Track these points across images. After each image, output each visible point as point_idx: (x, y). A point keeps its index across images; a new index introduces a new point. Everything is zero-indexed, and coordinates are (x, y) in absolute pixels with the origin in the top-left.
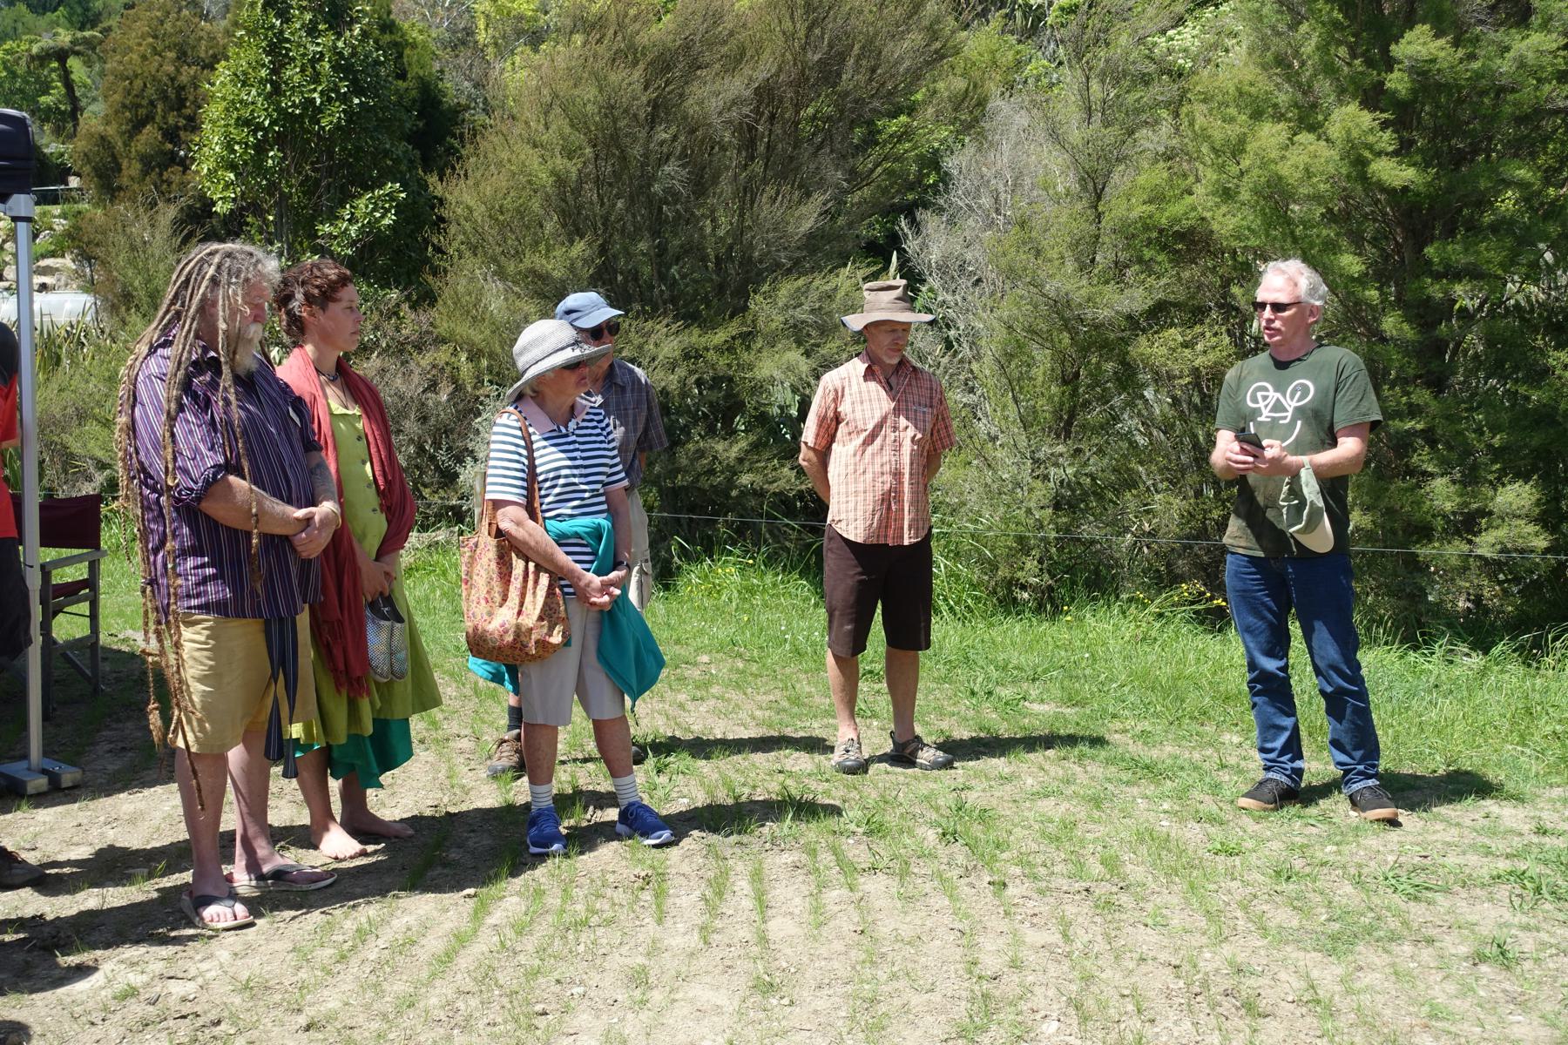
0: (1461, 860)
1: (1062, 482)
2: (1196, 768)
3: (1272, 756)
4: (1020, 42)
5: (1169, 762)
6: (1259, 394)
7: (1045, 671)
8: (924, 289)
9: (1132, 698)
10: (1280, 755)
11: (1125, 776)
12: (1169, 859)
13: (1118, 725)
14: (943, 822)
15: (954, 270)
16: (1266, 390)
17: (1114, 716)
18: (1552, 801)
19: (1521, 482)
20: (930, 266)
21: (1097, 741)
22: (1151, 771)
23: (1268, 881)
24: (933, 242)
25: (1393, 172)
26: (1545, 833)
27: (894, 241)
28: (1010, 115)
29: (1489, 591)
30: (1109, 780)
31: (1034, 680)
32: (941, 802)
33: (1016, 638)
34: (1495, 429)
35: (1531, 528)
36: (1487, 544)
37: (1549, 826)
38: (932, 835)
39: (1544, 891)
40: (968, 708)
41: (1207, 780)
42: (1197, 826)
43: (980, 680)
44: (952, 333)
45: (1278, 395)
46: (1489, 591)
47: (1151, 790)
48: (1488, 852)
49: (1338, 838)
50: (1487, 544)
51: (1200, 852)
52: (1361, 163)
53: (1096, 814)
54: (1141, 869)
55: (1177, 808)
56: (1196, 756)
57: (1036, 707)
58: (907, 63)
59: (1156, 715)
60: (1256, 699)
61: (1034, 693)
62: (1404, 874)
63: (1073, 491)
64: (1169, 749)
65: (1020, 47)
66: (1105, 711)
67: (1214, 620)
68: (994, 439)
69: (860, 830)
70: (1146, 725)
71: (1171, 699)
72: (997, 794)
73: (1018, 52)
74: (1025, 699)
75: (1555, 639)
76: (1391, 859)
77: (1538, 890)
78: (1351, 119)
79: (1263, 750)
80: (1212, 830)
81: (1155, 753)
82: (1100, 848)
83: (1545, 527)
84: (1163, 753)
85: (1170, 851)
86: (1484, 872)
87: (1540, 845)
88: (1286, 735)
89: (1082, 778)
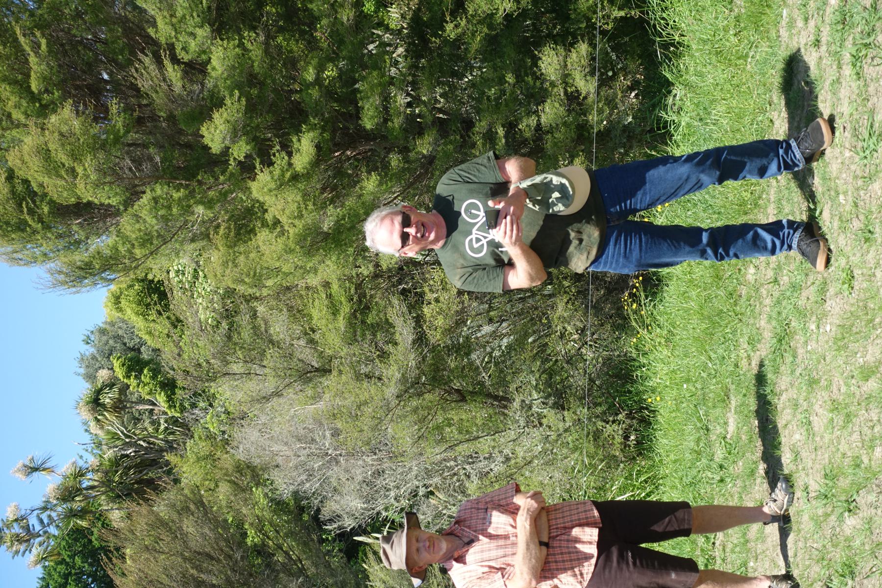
0: (846, 102)
1: (544, 403)
2: (779, 302)
3: (778, 243)
4: (192, 437)
5: (774, 323)
6: (476, 246)
7: (700, 420)
8: (384, 514)
9: (720, 351)
10: (779, 238)
11: (789, 359)
12: (859, 325)
13: (744, 363)
14: (839, 511)
15: (370, 488)
16: (471, 240)
17: (737, 366)
18: (791, 36)
19: (540, 62)
20: (365, 509)
21: (760, 379)
22: (783, 337)
23: (873, 248)
24: (347, 507)
25: (305, 147)
26: (818, 41)
27: (344, 536)
28: (249, 443)
29: (623, 81)
30: (793, 372)
31: (708, 430)
32: (820, 512)
33: (671, 442)
34: (502, 80)
35: (574, 55)
36: (586, 86)
37: (812, 38)
38: (851, 522)
39: (867, 41)
40: (735, 485)
41: (788, 293)
42: (829, 303)
43: (709, 475)
44: (422, 491)
45: (474, 231)
46: (623, 81)
47: (800, 338)
48: (838, 81)
49: (833, 193)
50: (586, 86)
51: (852, 301)
52: (295, 177)
53: (823, 383)
54: (870, 348)
55: (814, 318)
56: (768, 301)
57: (732, 428)
58: (206, 530)
59: (734, 332)
60: (731, 253)
61: (719, 430)
62: (860, 144)
63: (549, 395)
64: (763, 323)
65: (196, 436)
66: (732, 374)
67: (653, 285)
68: (508, 459)
69: (850, 582)
70: (743, 341)
71: (719, 321)
72: (810, 464)
73: (200, 438)
74: (725, 438)
75: (661, 36)
76: (848, 154)
77: (867, 46)
78: (261, 187)
79: (773, 252)
80: (832, 291)
81: (767, 335)
82: (854, 381)
83: (572, 45)
84: (767, 328)
85: (852, 325)
86: (854, 85)
87: (829, 44)
88: (760, 231)
89: (793, 393)
